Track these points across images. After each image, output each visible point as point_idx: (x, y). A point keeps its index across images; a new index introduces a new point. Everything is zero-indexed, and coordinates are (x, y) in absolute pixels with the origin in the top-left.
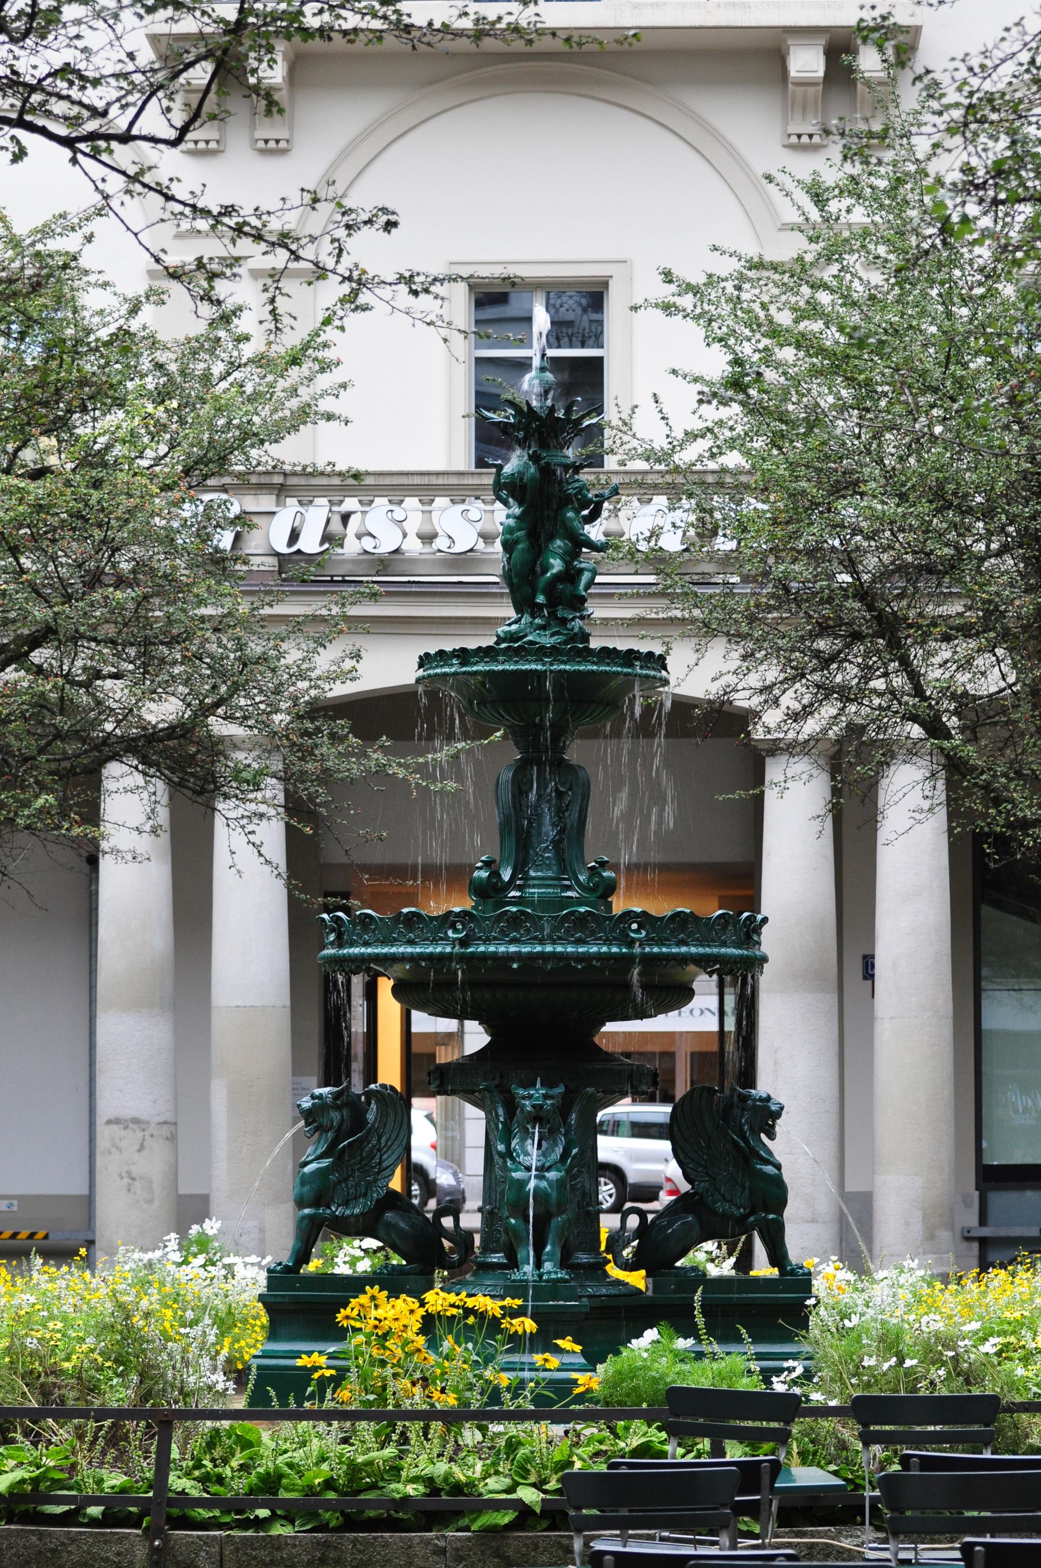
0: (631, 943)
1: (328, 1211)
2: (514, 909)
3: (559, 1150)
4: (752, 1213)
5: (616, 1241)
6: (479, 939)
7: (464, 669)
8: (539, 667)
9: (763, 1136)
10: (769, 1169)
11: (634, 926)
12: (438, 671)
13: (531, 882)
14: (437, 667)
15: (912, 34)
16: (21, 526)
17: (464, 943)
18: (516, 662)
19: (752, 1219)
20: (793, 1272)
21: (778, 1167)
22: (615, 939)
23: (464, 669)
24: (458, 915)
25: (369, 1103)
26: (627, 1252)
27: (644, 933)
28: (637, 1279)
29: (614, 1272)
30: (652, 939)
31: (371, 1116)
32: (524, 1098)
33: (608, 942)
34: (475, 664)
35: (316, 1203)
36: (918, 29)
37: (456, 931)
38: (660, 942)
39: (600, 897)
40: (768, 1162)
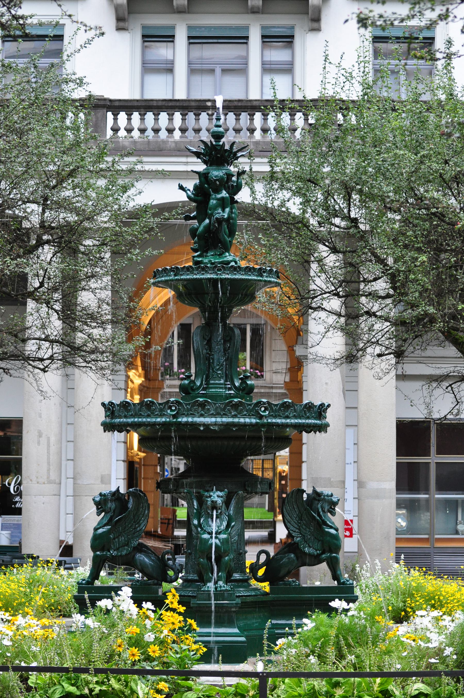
0: (261, 417)
1: (109, 553)
2: (201, 400)
3: (225, 524)
4: (323, 553)
5: (254, 568)
6: (184, 414)
7: (176, 278)
8: (215, 277)
9: (329, 514)
10: (333, 531)
11: (263, 409)
12: (163, 279)
13: (210, 386)
14: (162, 277)
15: (14, 428)
16: (229, 388)
17: (174, 416)
18: (203, 274)
19: (323, 556)
20: (344, 583)
21: (337, 530)
22: (253, 415)
23: (176, 278)
24: (172, 402)
25: (129, 498)
26: (261, 572)
27: (267, 413)
28: (265, 586)
29: (253, 582)
30: (272, 415)
31: (130, 505)
32: (207, 497)
33: (249, 416)
34: (181, 275)
35: (102, 550)
36: (19, 423)
37: (172, 411)
38: (275, 417)
39: (246, 394)
40: (331, 527)
